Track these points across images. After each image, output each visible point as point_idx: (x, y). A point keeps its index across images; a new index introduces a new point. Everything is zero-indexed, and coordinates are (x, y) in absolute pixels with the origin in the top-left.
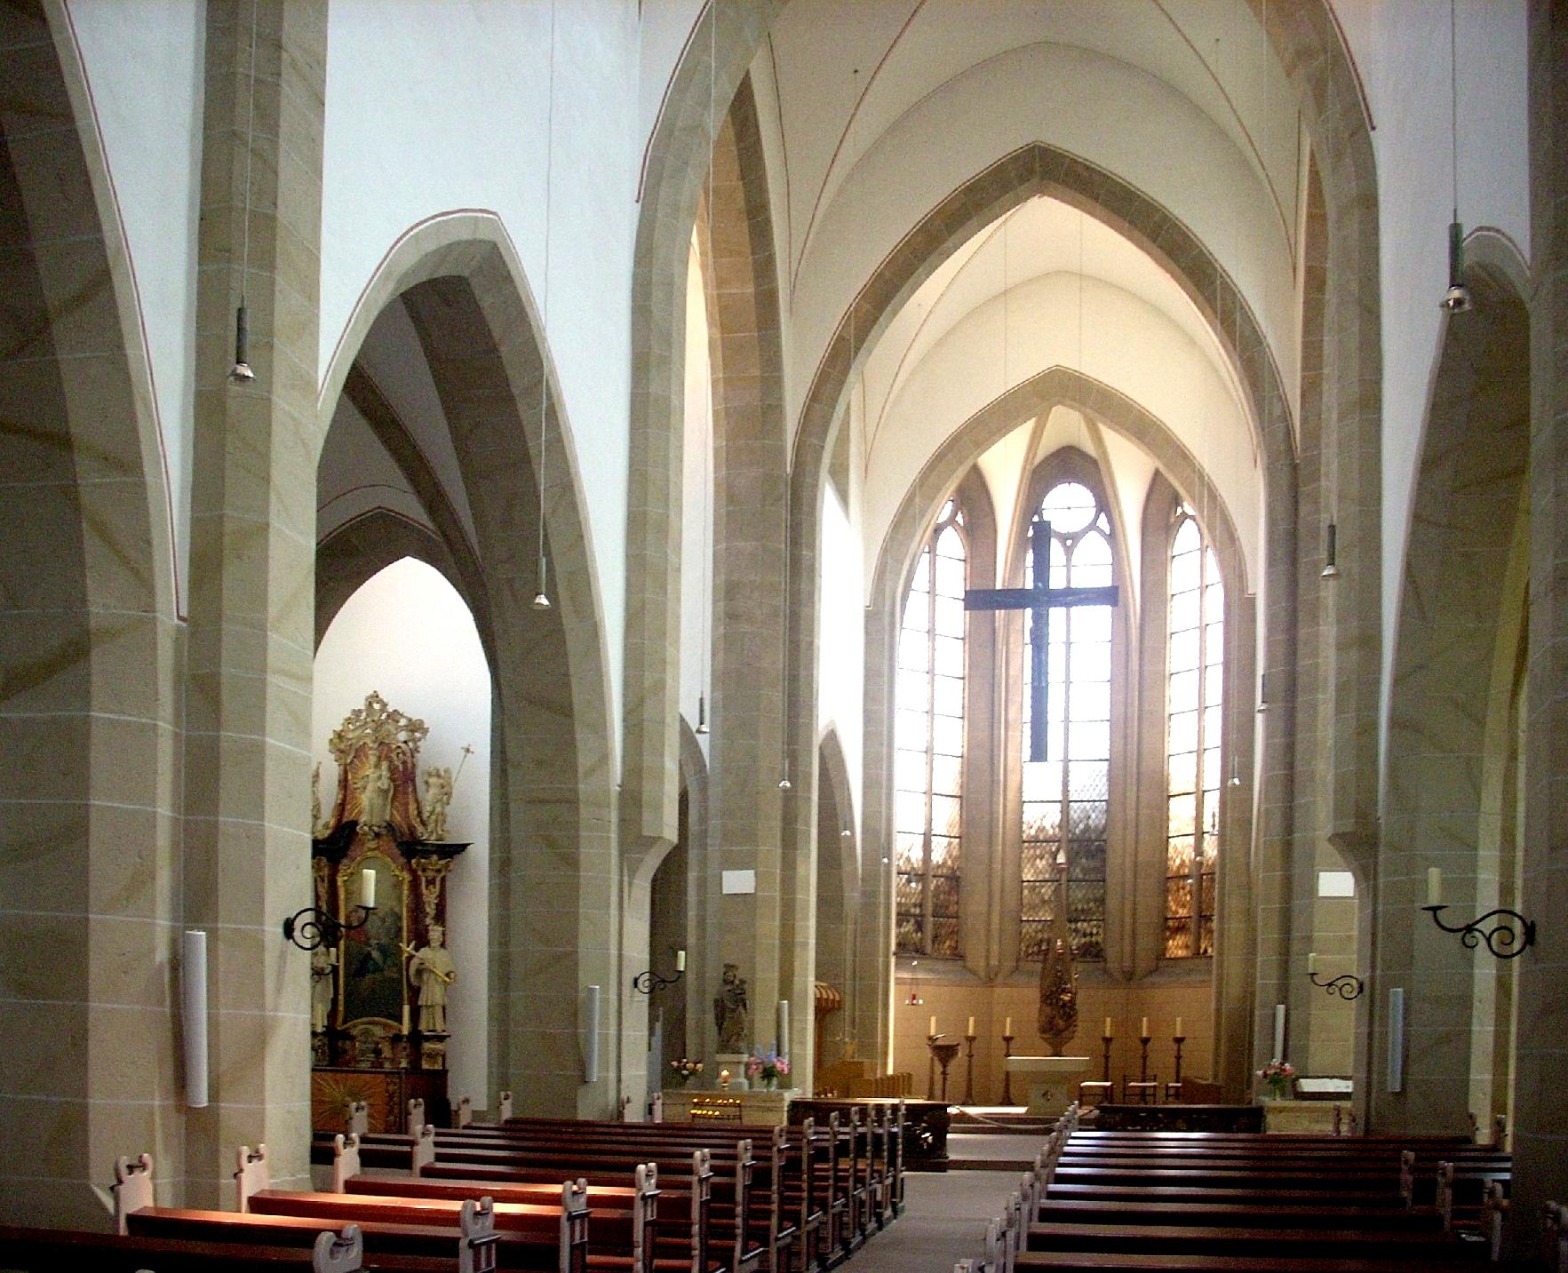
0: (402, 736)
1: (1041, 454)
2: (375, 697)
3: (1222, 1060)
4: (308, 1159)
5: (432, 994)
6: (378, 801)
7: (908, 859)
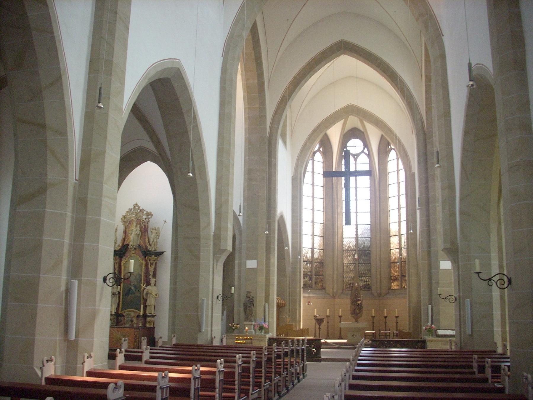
0: (144, 217)
1: (346, 130)
5: (151, 301)
7: (307, 257)
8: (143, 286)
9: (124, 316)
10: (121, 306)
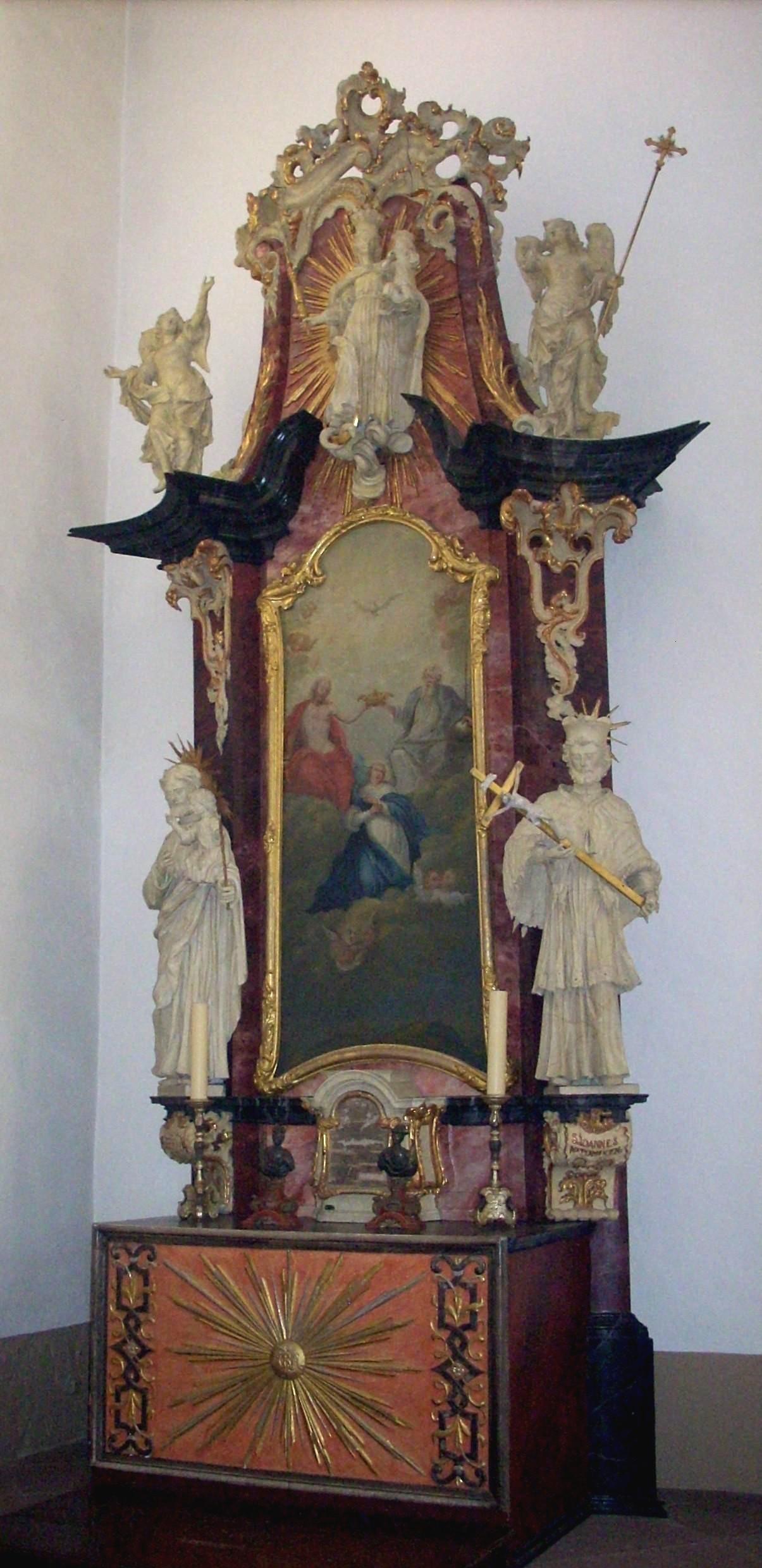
0: (450, 168)
2: (369, 80)
4: (545, 935)
6: (386, 353)
10: (272, 1018)
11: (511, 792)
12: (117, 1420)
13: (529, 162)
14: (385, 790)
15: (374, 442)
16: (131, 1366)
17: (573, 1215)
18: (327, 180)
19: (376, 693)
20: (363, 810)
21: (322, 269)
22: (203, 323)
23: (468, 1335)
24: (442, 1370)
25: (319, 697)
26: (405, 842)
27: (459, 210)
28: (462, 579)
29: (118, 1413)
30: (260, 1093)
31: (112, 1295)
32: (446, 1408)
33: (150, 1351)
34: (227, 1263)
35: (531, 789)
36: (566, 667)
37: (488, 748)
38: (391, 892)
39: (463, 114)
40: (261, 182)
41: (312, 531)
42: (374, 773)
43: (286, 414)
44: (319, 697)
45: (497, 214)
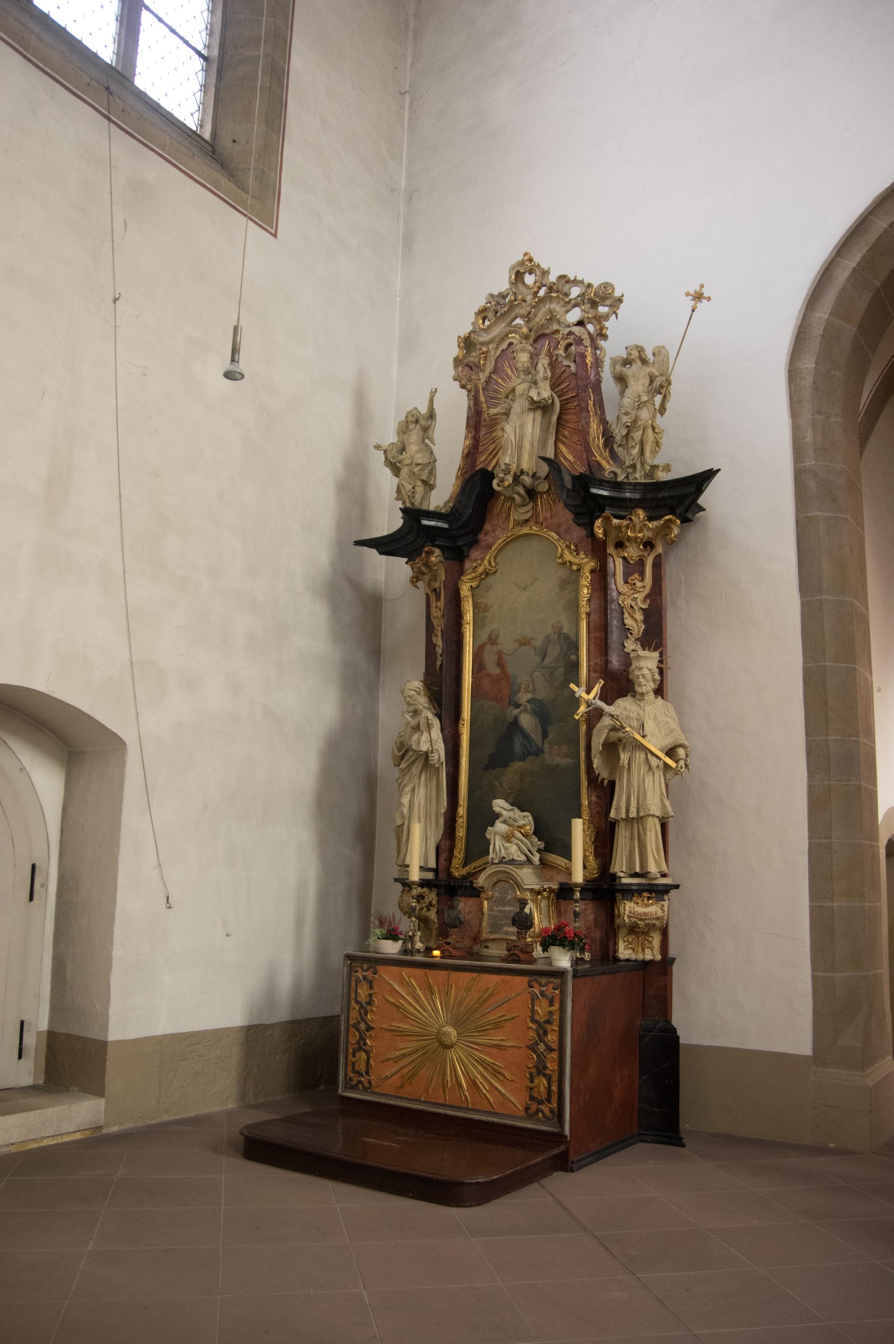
0: (575, 315)
3: (35, 1145)
5: (644, 791)
8: (587, 695)
9: (476, 893)
10: (461, 832)
11: (594, 699)
12: (353, 1068)
13: (622, 309)
14: (529, 696)
15: (524, 486)
16: (362, 1039)
17: (633, 957)
18: (503, 325)
19: (525, 637)
20: (516, 708)
21: (500, 381)
22: (431, 415)
23: (548, 1027)
24: (533, 1048)
25: (493, 640)
26: (540, 728)
27: (579, 341)
28: (575, 567)
29: (354, 1063)
30: (455, 878)
31: (353, 995)
32: (534, 1070)
33: (373, 1028)
34: (415, 978)
35: (608, 696)
36: (636, 620)
37: (589, 671)
38: (530, 758)
39: (582, 282)
40: (465, 329)
41: (491, 540)
42: (523, 686)
43: (478, 468)
44: (493, 640)
45: (602, 343)
